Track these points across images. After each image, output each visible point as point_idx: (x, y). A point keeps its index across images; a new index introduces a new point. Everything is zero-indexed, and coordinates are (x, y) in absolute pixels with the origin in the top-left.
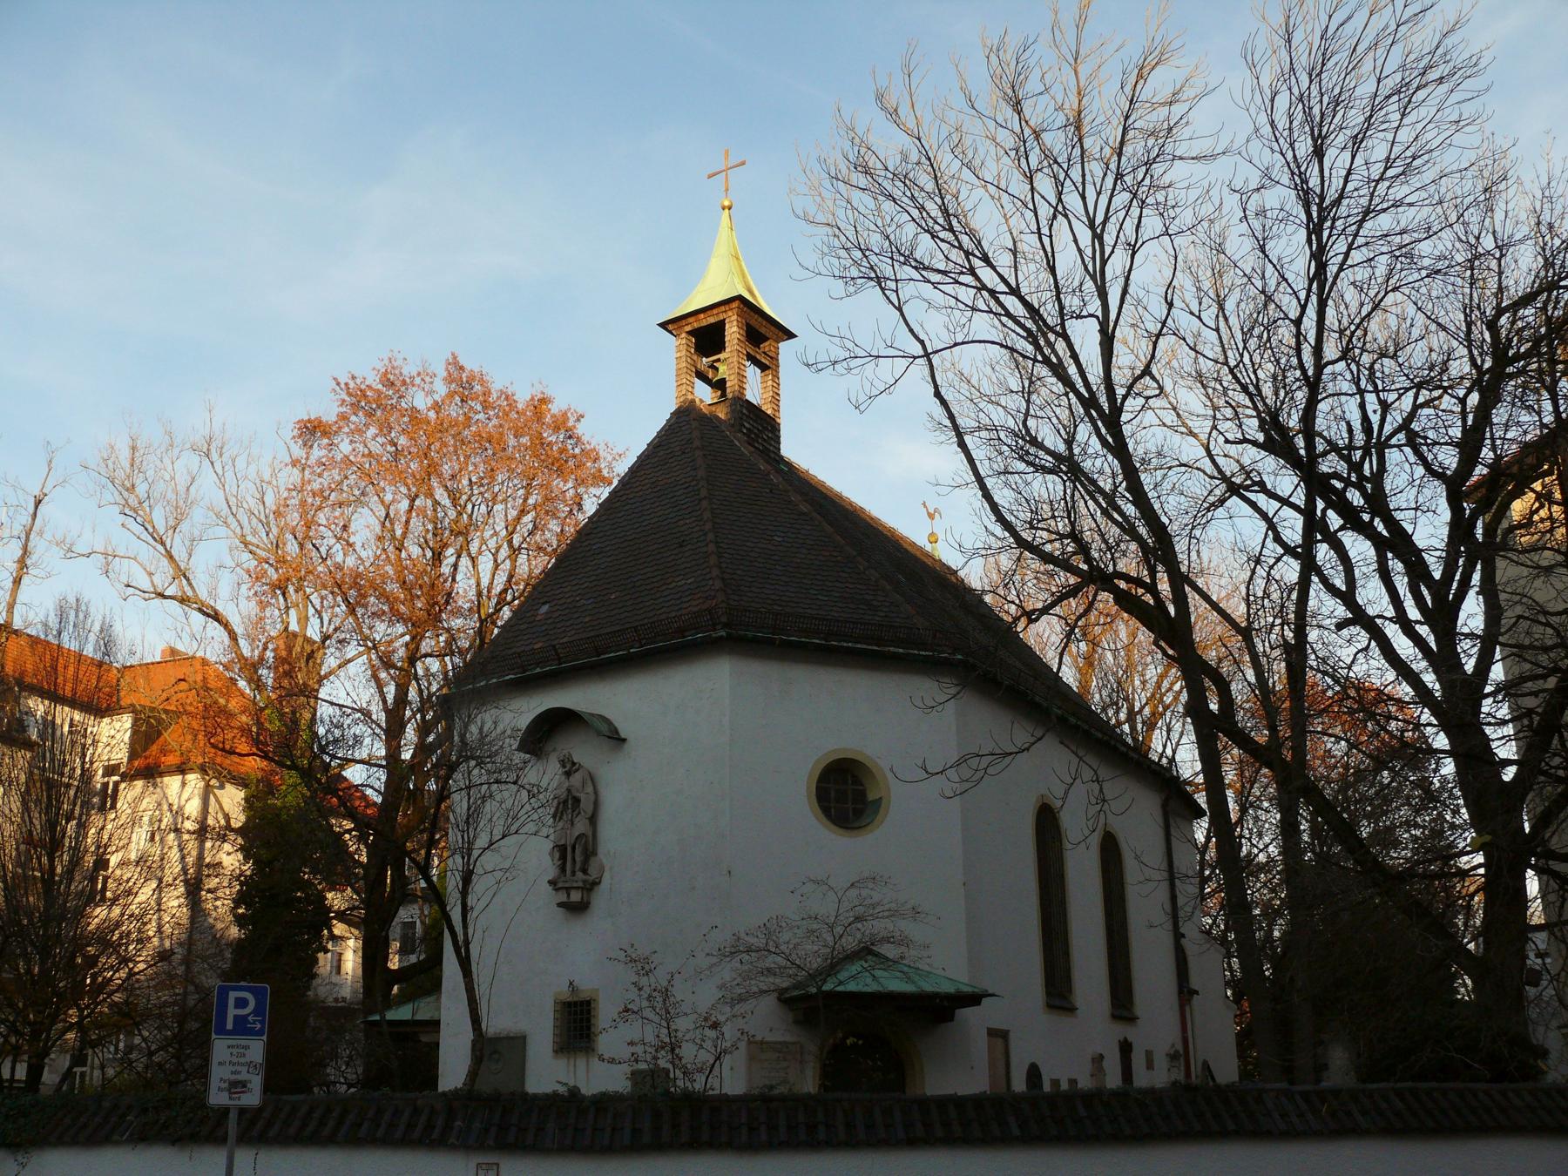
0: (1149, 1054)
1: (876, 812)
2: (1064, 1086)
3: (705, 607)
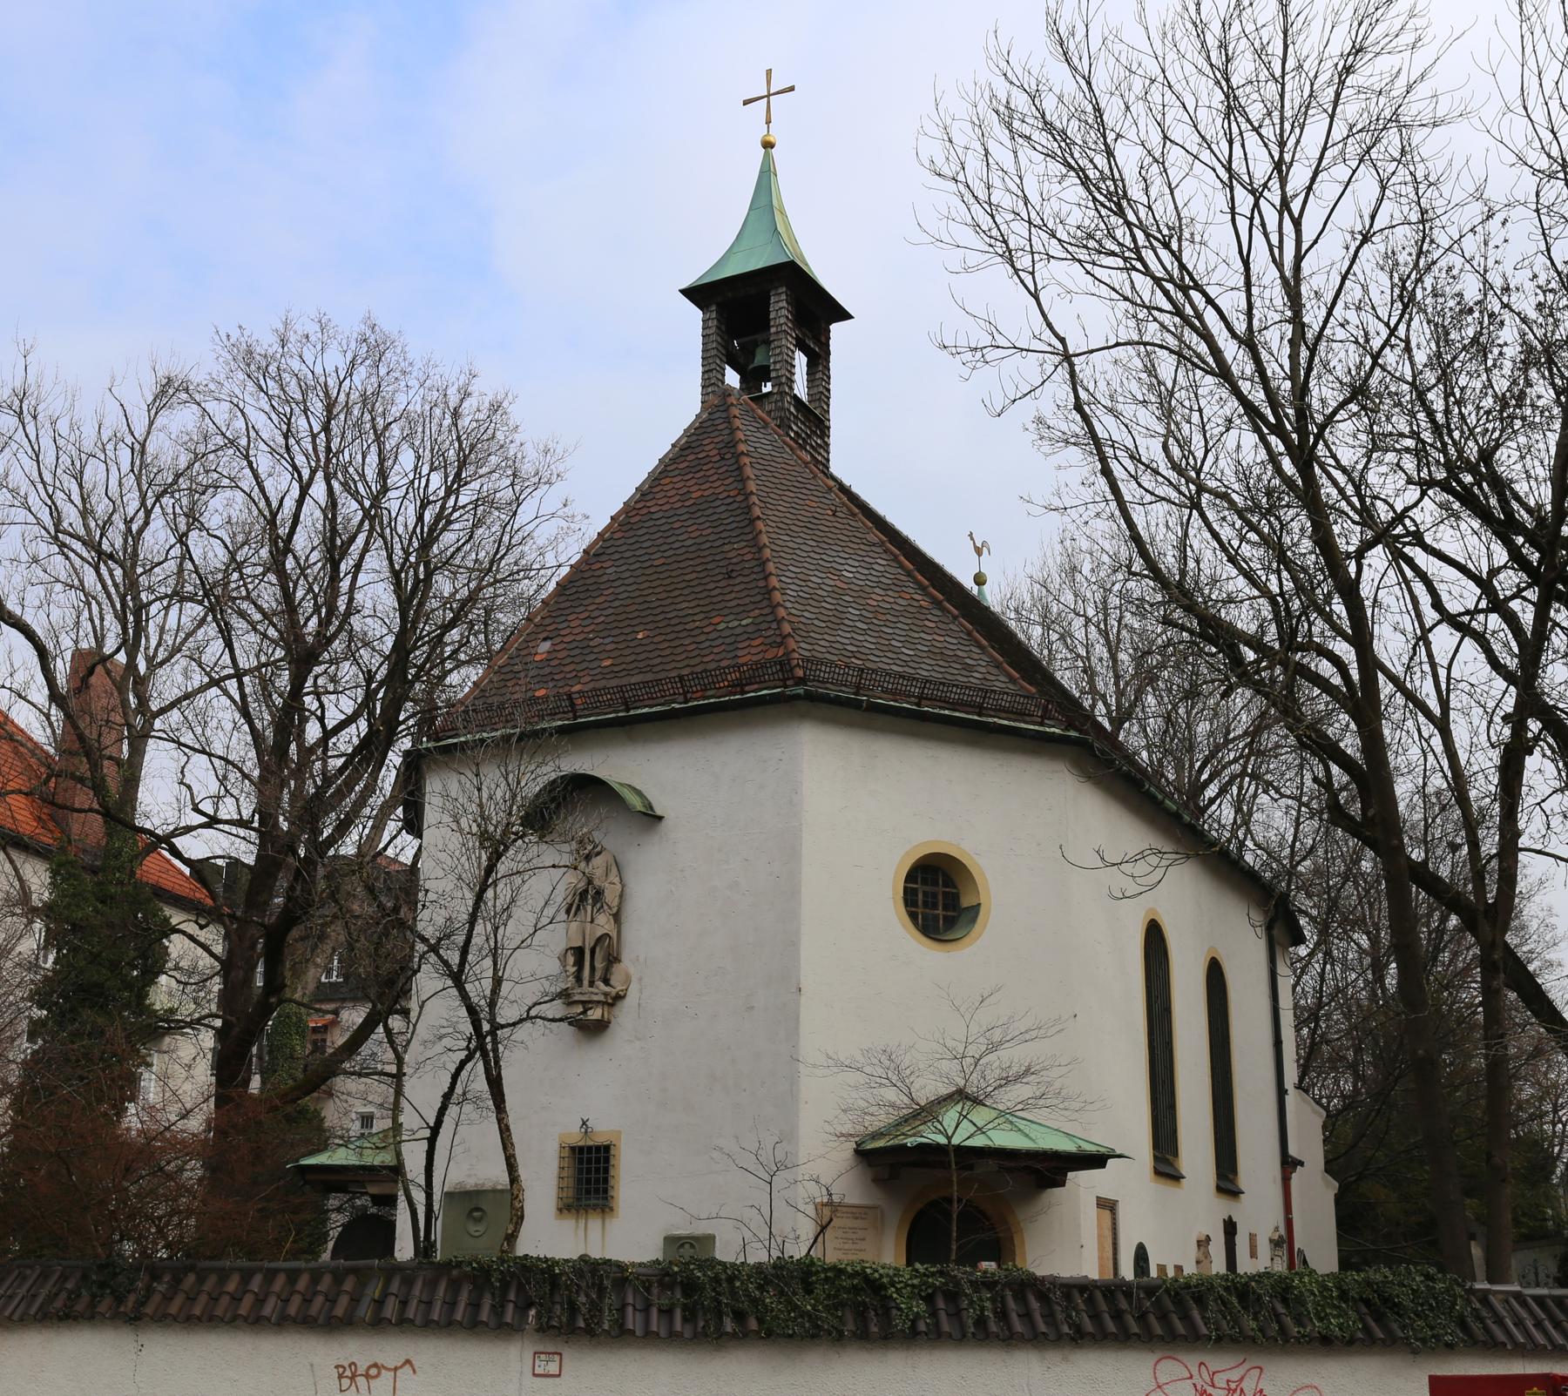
0: (1252, 1237)
1: (974, 920)
2: (1171, 1273)
3: (769, 655)
